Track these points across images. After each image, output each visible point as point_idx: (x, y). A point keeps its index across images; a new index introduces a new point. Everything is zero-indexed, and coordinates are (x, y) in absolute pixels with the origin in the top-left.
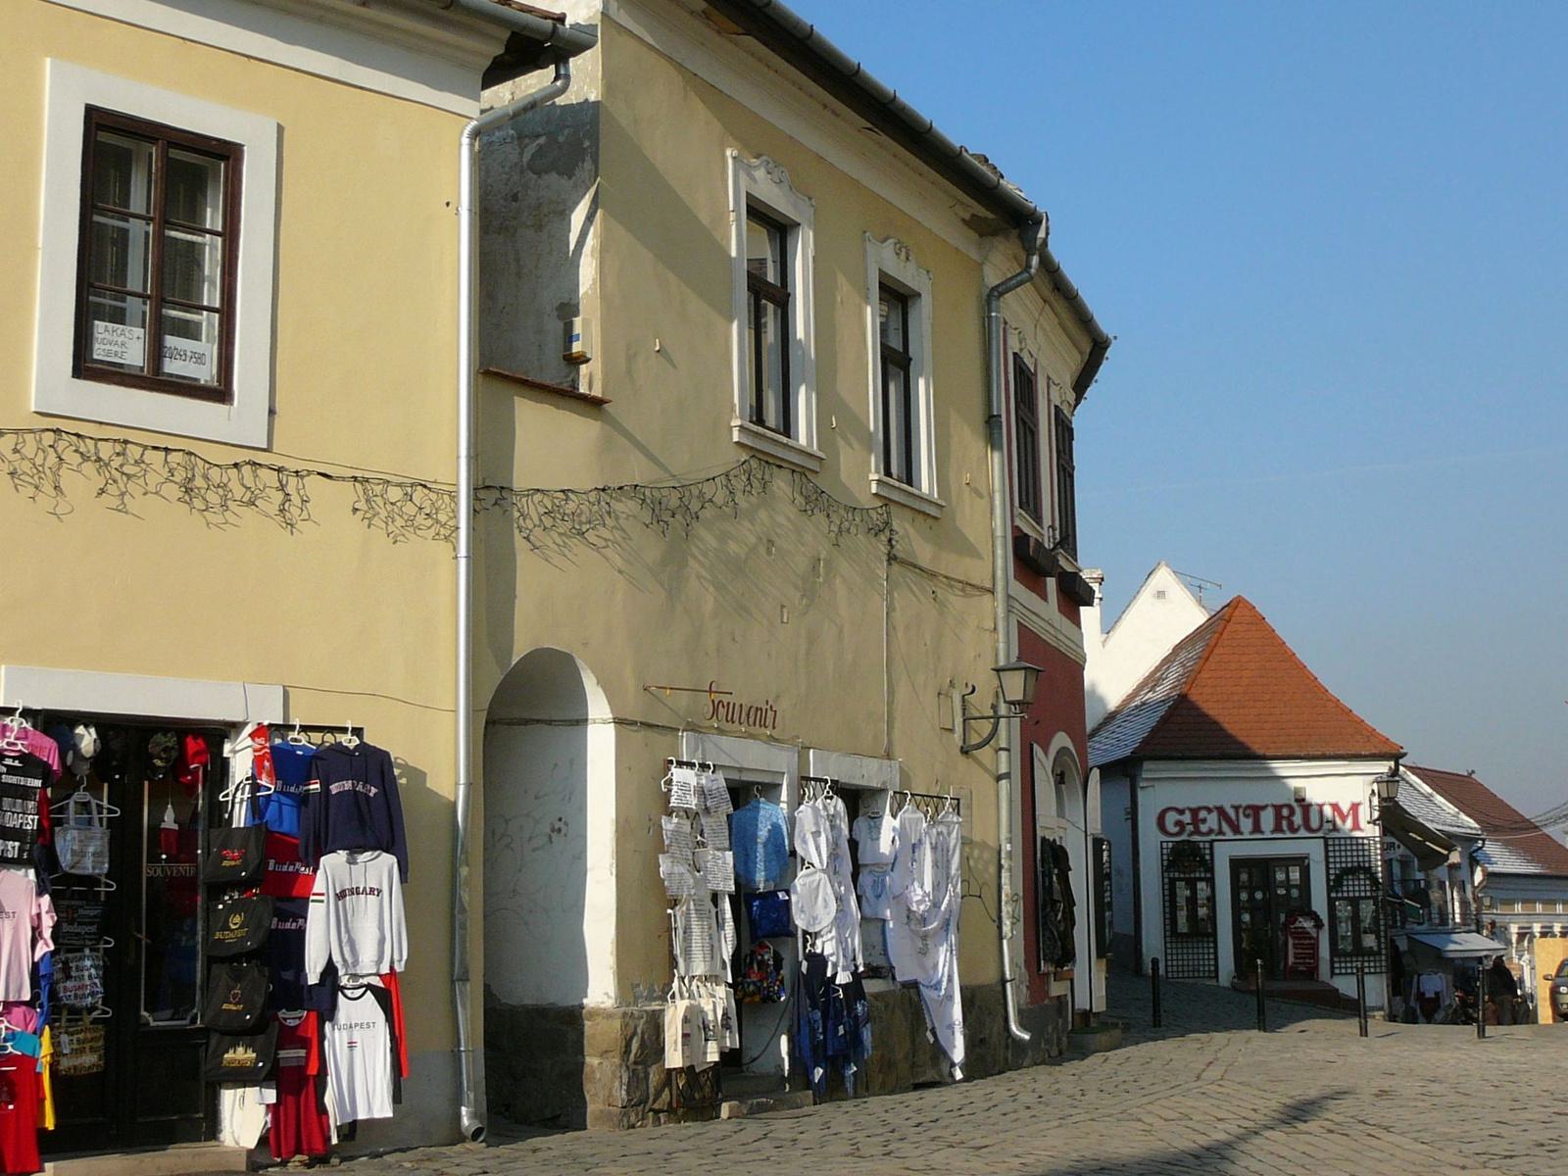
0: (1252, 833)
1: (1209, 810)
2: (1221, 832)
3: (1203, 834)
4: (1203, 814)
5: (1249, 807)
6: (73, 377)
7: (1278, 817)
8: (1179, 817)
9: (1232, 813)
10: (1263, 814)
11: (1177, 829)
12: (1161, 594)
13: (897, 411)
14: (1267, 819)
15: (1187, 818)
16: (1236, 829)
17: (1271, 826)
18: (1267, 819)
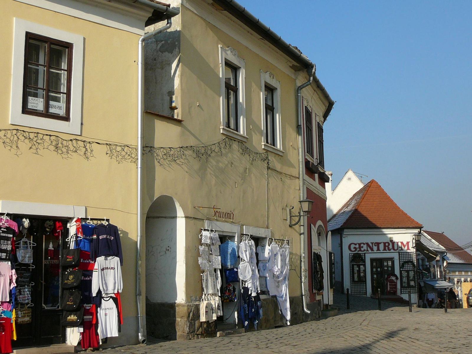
0: (377, 251)
1: (364, 244)
2: (367, 251)
3: (362, 251)
4: (362, 245)
5: (376, 243)
6: (22, 113)
7: (385, 246)
8: (355, 246)
9: (371, 245)
10: (380, 245)
11: (354, 250)
12: (349, 179)
13: (270, 124)
14: (382, 247)
15: (357, 246)
16: (372, 250)
17: (383, 249)
18: (382, 247)
